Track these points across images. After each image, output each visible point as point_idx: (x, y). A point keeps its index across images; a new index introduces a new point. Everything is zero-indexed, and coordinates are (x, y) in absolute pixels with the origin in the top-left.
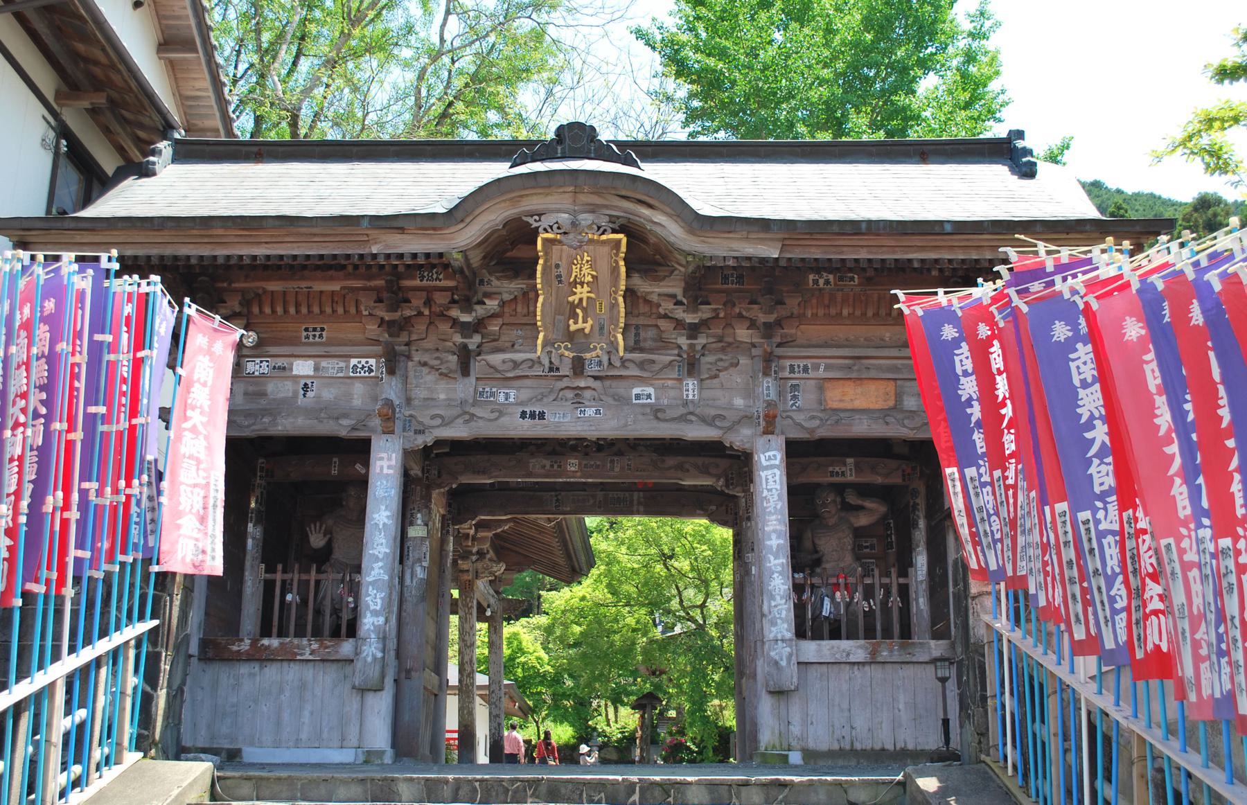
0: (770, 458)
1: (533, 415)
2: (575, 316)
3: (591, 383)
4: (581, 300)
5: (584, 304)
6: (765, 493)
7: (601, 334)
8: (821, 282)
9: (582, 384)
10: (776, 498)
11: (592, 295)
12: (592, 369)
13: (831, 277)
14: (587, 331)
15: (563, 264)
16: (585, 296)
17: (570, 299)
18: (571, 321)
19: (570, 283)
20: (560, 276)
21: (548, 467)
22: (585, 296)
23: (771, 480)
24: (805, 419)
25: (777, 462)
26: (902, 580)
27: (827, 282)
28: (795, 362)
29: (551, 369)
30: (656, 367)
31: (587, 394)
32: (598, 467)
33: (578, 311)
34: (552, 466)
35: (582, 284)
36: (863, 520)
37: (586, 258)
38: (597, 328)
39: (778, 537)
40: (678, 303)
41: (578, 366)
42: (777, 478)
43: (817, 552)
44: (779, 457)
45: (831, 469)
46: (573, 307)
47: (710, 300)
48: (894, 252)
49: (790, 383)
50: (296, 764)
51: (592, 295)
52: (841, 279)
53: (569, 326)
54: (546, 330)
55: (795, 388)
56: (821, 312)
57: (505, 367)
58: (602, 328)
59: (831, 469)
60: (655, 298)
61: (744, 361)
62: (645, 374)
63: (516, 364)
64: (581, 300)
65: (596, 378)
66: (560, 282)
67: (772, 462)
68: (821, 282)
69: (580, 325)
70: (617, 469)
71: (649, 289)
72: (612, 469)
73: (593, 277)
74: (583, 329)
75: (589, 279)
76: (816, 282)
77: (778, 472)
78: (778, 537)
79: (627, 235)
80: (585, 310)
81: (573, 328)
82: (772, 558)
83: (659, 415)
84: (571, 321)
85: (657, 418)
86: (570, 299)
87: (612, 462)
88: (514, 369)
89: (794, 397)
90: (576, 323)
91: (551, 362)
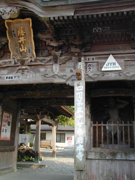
0: (79, 88)
1: (9, 78)
2: (21, 47)
3: (27, 67)
4: (22, 41)
5: (23, 43)
6: (77, 100)
7: (30, 52)
8: (97, 30)
9: (24, 68)
10: (81, 101)
11: (25, 40)
12: (26, 63)
13: (100, 29)
14: (25, 51)
15: (15, 31)
16: (23, 40)
17: (19, 42)
18: (20, 49)
19: (18, 36)
20: (15, 34)
21: (31, 94)
22: (23, 40)
23: (80, 96)
24: (93, 74)
25: (82, 89)
26: (130, 125)
27: (99, 30)
28: (90, 57)
29: (15, 64)
30: (46, 61)
31: (26, 71)
32: (44, 93)
33: (22, 45)
34: (32, 93)
35: (21, 36)
36: (121, 106)
37: (22, 28)
38: (28, 50)
39: (81, 115)
40: (52, 41)
41: (23, 63)
42: (82, 95)
43: (109, 115)
44: (82, 88)
45: (109, 92)
46: (20, 44)
47: (61, 39)
48: (117, 10)
49: (88, 64)
50: (66, 130)
51: (25, 40)
52: (104, 29)
53: (20, 50)
54: (13, 52)
55: (90, 65)
56: (98, 41)
57: (3, 64)
58: (29, 50)
59: (109, 92)
60: (44, 40)
61: (73, 58)
62: (42, 63)
63: (6, 63)
64: (22, 41)
65: (29, 66)
66: (15, 36)
67: (80, 90)
68: (97, 30)
69: (23, 50)
70: (49, 94)
71: (44, 37)
72: (48, 94)
73: (24, 34)
74: (24, 51)
75: (23, 34)
76: (95, 31)
77: (82, 93)
78: (81, 115)
79: (31, 18)
80: (24, 45)
81: (21, 51)
82: (79, 122)
83: (46, 76)
84: (20, 49)
85: (46, 77)
86: (19, 42)
87: (48, 92)
88: (5, 64)
89: (90, 68)
90: (22, 49)
91: (15, 62)
